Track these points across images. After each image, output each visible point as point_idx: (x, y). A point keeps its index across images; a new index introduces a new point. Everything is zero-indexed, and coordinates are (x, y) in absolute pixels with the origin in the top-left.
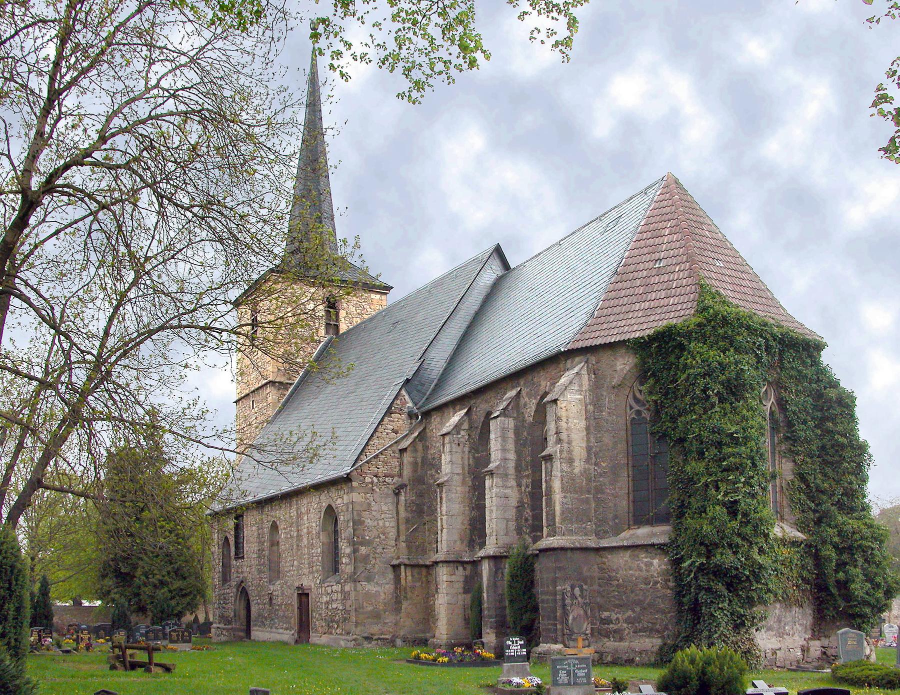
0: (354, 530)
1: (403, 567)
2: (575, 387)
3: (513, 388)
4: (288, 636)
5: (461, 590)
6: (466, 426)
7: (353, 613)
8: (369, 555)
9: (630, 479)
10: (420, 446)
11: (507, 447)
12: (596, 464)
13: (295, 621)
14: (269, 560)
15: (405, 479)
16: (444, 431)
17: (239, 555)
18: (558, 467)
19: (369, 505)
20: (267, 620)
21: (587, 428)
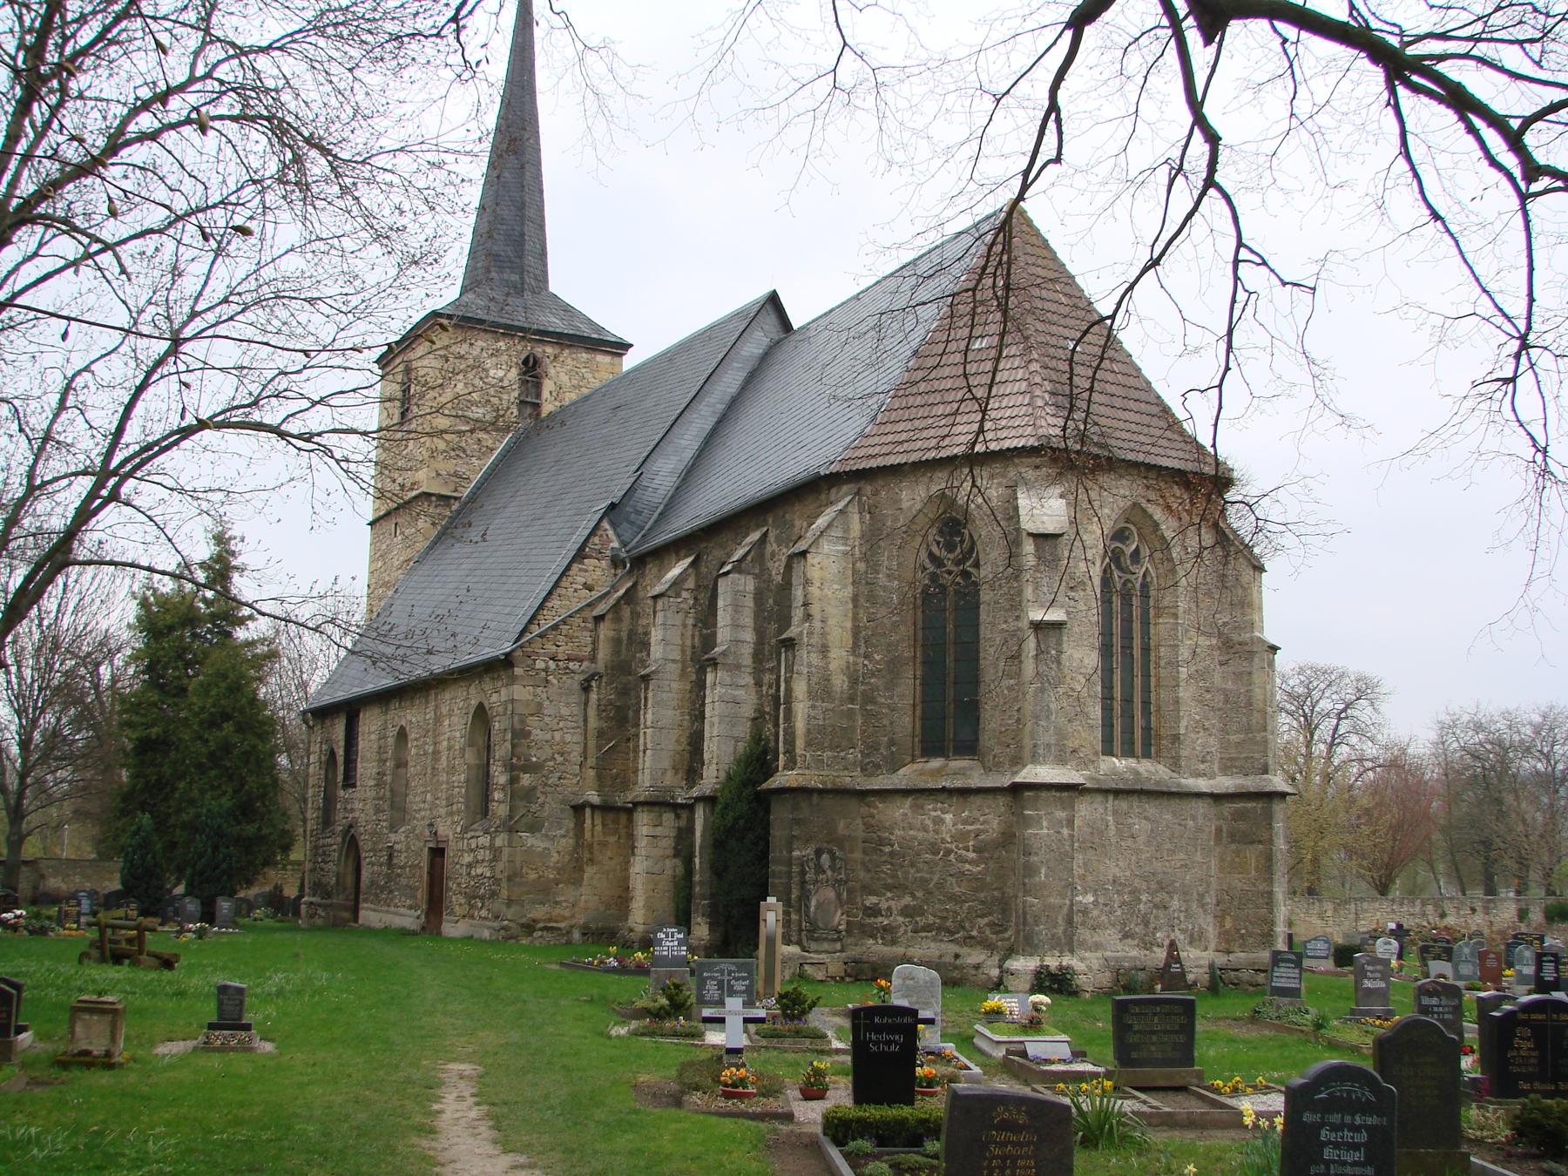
0: (513, 746)
1: (588, 811)
2: (836, 532)
3: (758, 527)
4: (408, 918)
5: (670, 852)
6: (690, 584)
7: (504, 884)
8: (535, 788)
10: (626, 612)
11: (741, 622)
12: (866, 657)
13: (422, 895)
14: (392, 790)
16: (658, 590)
17: (349, 782)
18: (807, 658)
19: (540, 705)
20: (384, 892)
21: (855, 598)
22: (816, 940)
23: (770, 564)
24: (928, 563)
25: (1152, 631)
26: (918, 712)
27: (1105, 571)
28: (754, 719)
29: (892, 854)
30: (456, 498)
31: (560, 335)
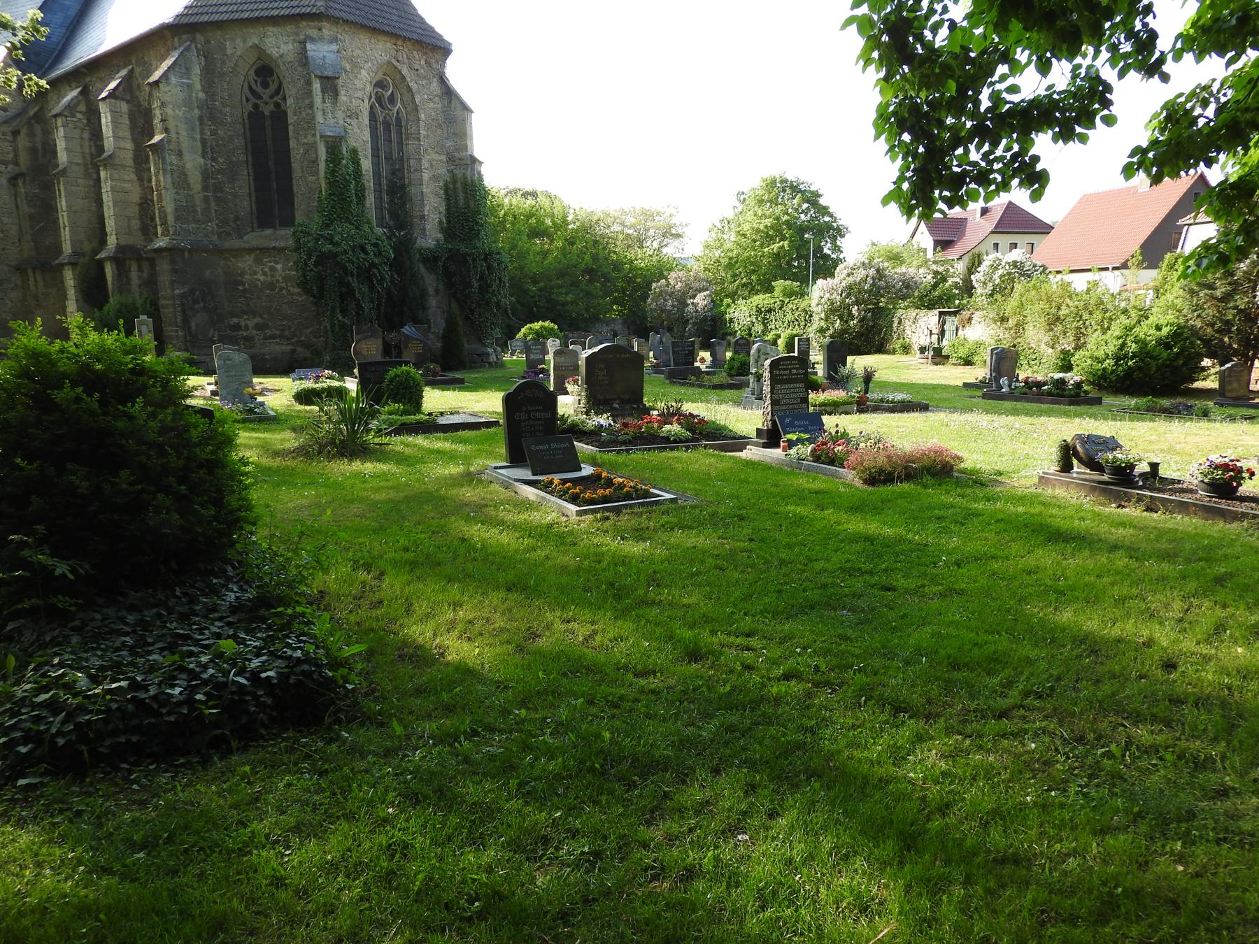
12: (213, 159)
23: (137, 93)
24: (250, 96)
26: (253, 198)
27: (371, 107)
28: (140, 205)
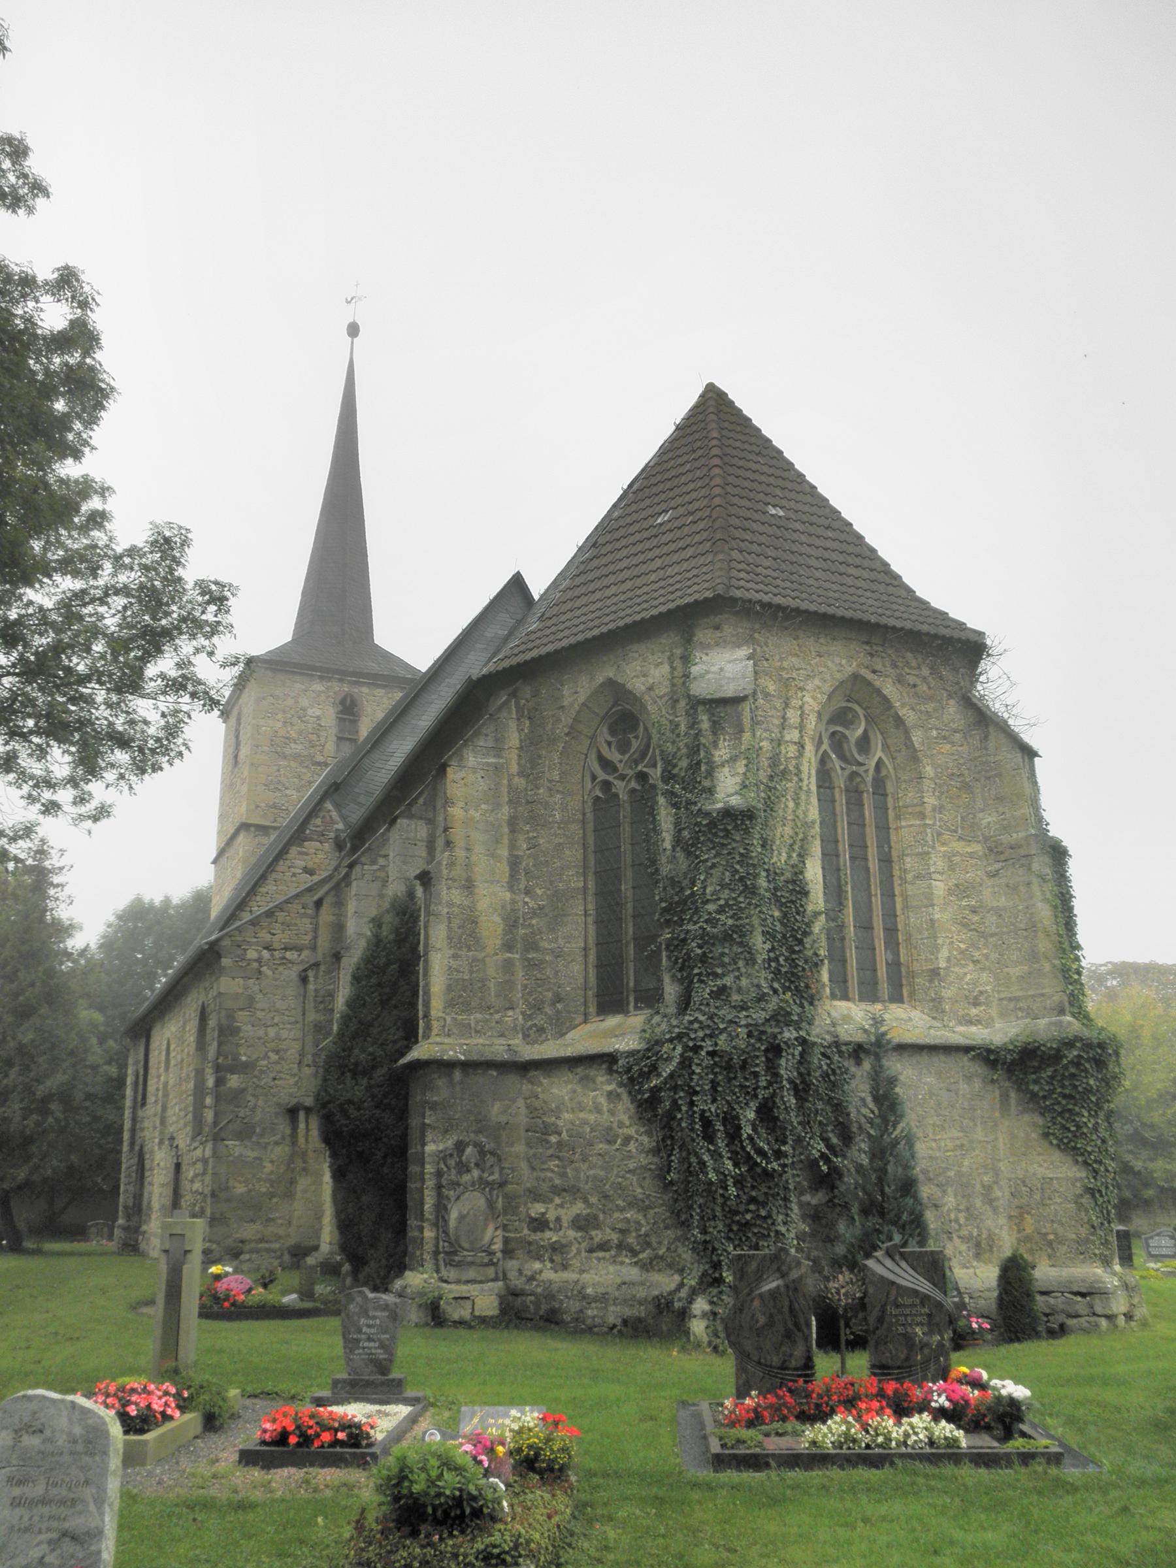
1: (302, 1115)
9: (590, 920)
12: (528, 892)
15: (319, 956)
19: (251, 999)
22: (458, 1265)
25: (893, 838)
26: (592, 958)
29: (560, 1144)
30: (275, 828)
31: (375, 676)
